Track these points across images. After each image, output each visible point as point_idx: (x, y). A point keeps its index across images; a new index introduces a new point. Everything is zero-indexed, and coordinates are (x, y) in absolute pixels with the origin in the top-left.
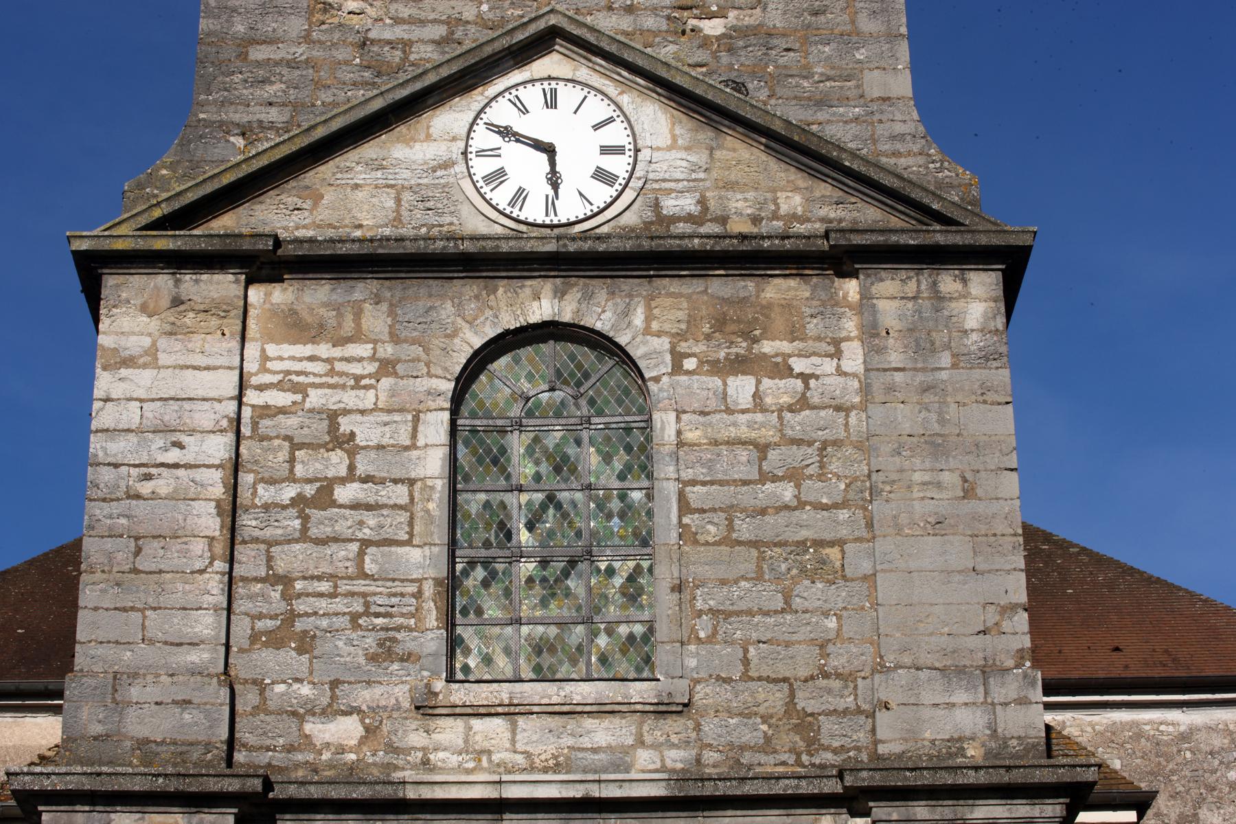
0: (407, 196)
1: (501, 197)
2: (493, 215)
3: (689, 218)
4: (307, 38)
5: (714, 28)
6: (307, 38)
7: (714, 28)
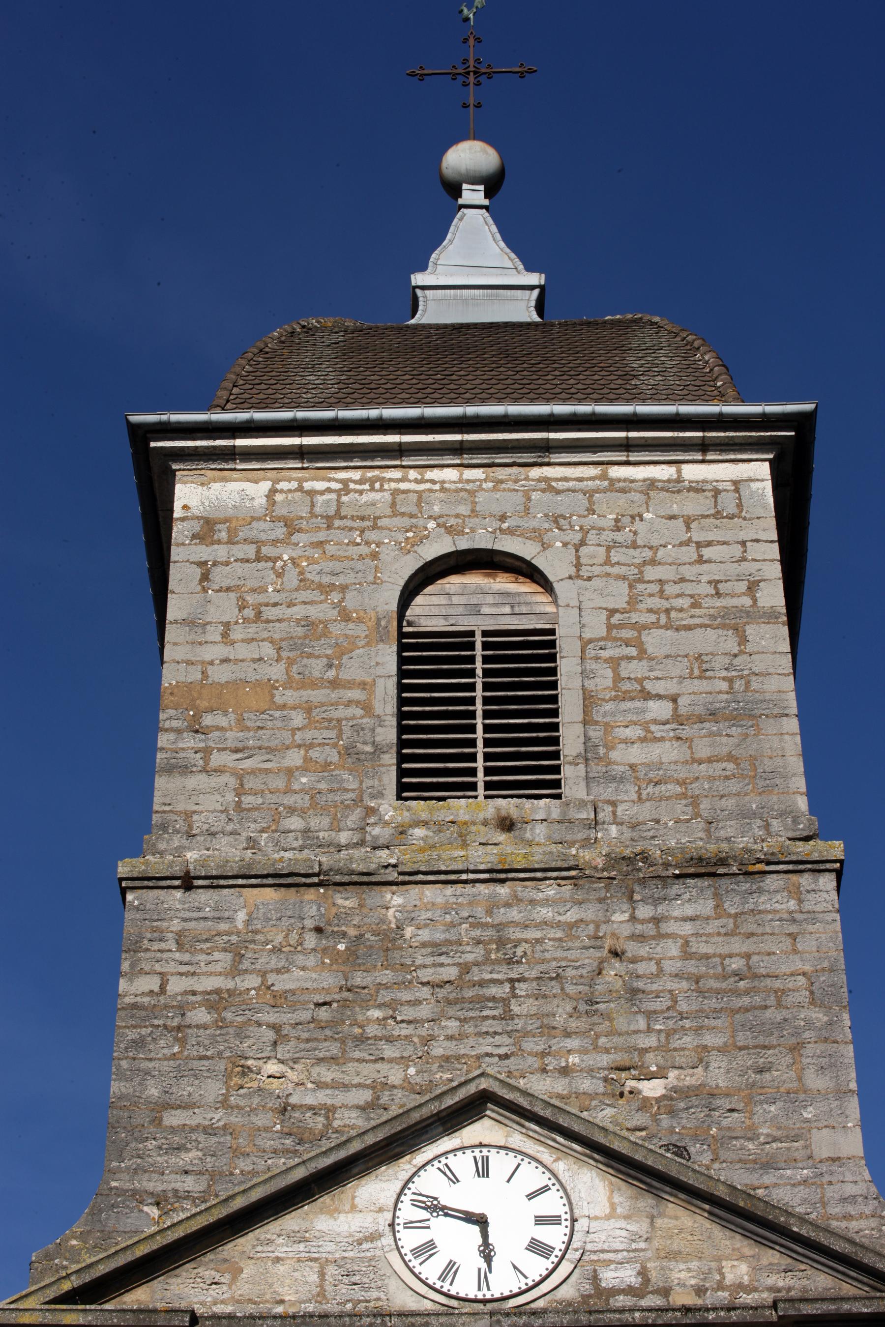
0: (331, 1270)
1: (431, 1270)
2: (423, 1289)
3: (630, 1291)
4: (224, 1103)
5: (652, 1089)
6: (224, 1103)
7: (652, 1089)
